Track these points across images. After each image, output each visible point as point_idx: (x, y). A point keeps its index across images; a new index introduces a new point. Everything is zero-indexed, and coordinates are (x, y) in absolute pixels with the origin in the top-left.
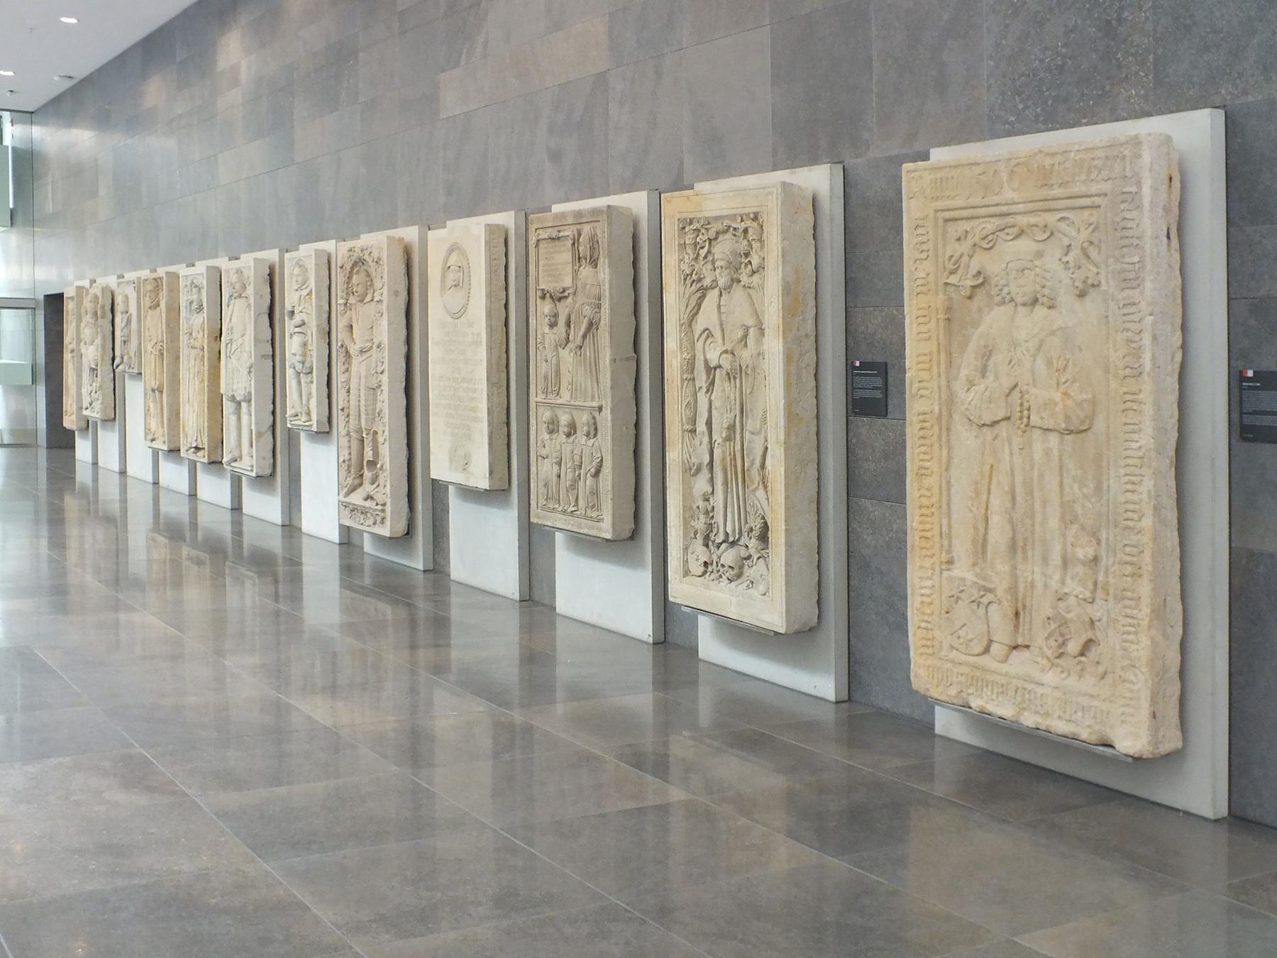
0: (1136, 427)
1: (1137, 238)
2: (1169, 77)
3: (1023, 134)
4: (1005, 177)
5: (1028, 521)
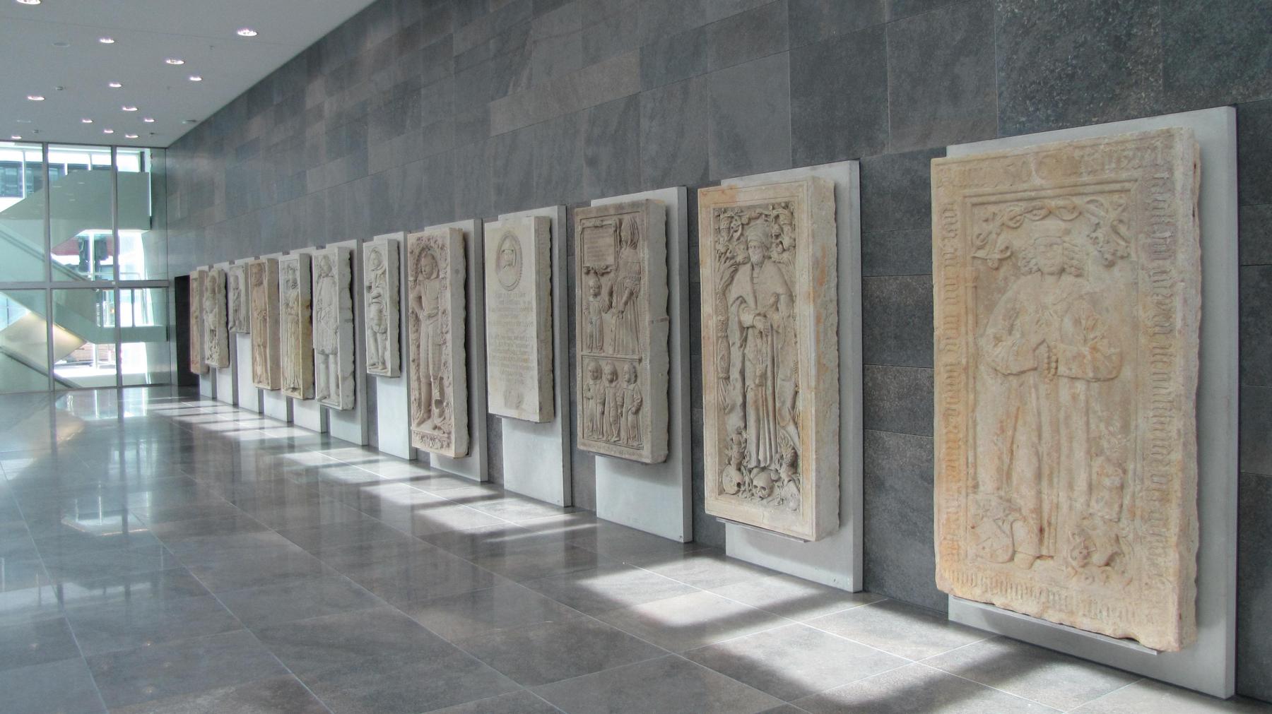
0: (1165, 376)
2: (1179, 82)
4: (1033, 167)
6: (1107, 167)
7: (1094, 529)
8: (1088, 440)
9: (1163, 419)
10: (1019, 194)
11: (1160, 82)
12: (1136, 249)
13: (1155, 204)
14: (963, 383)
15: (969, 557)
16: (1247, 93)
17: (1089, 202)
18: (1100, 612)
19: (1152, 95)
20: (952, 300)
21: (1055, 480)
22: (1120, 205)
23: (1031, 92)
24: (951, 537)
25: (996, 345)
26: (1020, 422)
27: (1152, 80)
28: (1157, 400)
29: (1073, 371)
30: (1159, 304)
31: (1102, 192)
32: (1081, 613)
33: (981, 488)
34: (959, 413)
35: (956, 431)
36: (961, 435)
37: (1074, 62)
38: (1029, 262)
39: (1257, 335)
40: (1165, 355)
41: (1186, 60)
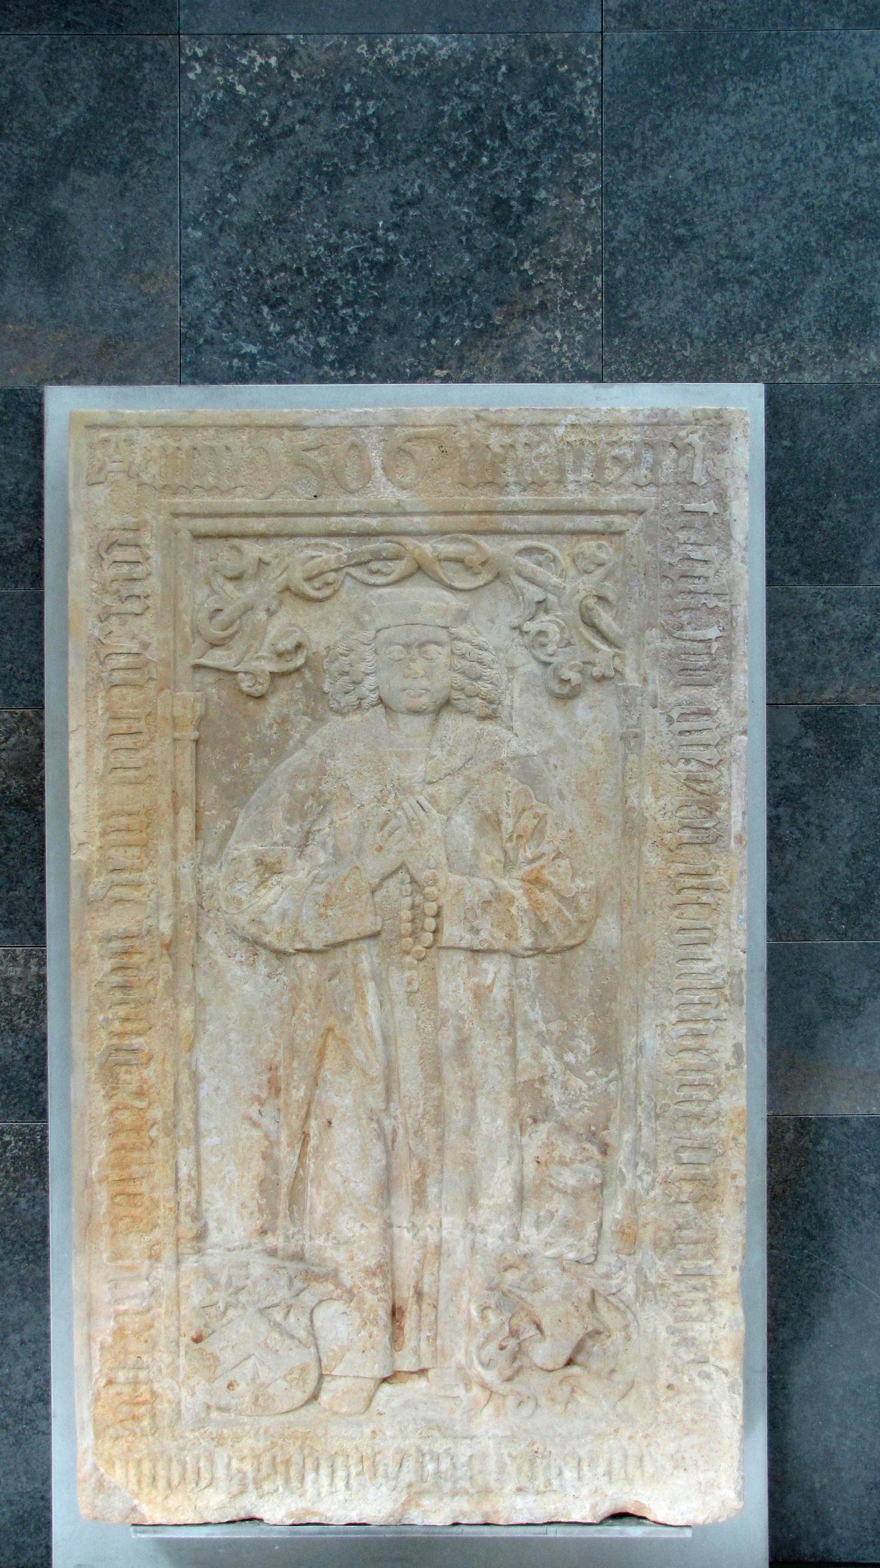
0: (706, 934)
1: (716, 594)
2: (640, 319)
3: (280, 382)
4: (376, 458)
5: (430, 1132)
6: (571, 477)
7: (537, 1287)
8: (514, 1091)
9: (700, 1026)
10: (334, 519)
11: (598, 314)
12: (638, 662)
13: (685, 566)
14: (161, 983)
15: (187, 1416)
16: (778, 364)
17: (523, 552)
18: (560, 1474)
19: (577, 338)
20: (131, 773)
21: (432, 1191)
22: (600, 565)
23: (275, 289)
24: (131, 1374)
25: (263, 883)
26: (332, 1062)
27: (580, 306)
28: (687, 985)
29: (484, 935)
30: (691, 780)
31: (552, 532)
32: (510, 1487)
33: (214, 1237)
34: (151, 1058)
35: (143, 1104)
36: (157, 1113)
37: (391, 237)
38: (356, 683)
39: (797, 840)
40: (706, 889)
41: (654, 278)
